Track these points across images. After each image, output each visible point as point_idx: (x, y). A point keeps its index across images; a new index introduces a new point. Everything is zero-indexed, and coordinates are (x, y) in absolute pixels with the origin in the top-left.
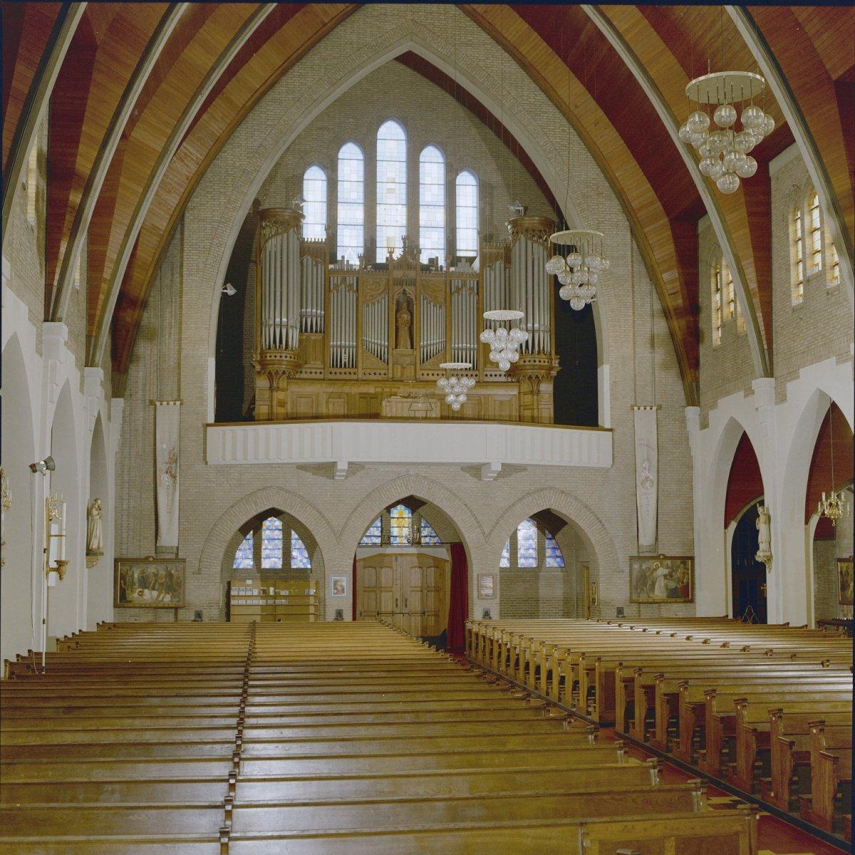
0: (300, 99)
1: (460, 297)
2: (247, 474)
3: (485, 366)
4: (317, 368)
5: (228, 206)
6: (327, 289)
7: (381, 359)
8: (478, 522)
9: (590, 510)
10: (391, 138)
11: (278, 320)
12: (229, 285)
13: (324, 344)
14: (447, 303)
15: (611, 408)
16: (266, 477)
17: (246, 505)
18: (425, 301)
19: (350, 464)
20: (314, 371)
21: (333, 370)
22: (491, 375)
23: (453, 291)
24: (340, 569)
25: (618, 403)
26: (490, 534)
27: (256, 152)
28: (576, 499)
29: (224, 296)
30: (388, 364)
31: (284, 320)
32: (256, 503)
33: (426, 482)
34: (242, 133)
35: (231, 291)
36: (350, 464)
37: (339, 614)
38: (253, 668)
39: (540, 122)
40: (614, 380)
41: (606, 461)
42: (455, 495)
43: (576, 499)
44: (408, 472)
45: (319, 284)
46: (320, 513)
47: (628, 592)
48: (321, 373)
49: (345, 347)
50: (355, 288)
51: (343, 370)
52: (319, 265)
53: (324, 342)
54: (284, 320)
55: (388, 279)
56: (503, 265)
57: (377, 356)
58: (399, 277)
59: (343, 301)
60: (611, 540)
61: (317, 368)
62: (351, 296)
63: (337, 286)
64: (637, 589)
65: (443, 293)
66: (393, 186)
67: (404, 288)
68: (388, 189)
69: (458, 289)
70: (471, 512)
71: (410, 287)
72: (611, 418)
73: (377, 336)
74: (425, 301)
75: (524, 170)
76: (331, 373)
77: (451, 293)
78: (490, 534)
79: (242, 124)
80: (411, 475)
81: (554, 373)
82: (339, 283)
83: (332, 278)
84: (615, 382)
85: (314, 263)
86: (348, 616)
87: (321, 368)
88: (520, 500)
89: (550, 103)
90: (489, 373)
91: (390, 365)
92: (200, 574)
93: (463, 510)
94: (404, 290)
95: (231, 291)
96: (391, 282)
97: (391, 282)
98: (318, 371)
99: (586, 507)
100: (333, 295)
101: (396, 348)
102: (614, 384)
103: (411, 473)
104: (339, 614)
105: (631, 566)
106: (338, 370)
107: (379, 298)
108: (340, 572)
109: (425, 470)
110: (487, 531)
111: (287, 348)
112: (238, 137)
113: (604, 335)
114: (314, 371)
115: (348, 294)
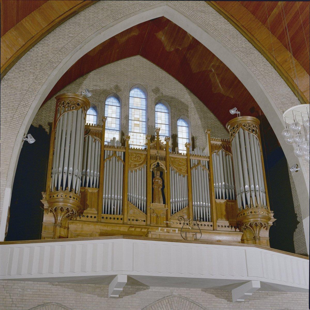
0: (93, 25)
1: (197, 170)
2: (29, 290)
3: (217, 219)
4: (93, 214)
5: (35, 81)
6: (102, 159)
7: (141, 209)
10: (137, 99)
11: (66, 168)
12: (29, 135)
13: (98, 195)
18: (173, 172)
19: (129, 278)
20: (90, 215)
21: (105, 216)
23: (192, 166)
27: (60, 51)
29: (26, 143)
30: (146, 214)
34: (51, 38)
35: (31, 140)
36: (129, 278)
39: (250, 58)
44: (172, 293)
45: (97, 154)
48: (95, 217)
49: (115, 199)
50: (122, 159)
51: (112, 216)
52: (97, 142)
53: (99, 194)
54: (71, 169)
55: (147, 155)
56: (224, 153)
57: (139, 208)
58: (154, 154)
59: (114, 168)
61: (93, 214)
62: (120, 165)
65: (185, 167)
66: (138, 123)
67: (158, 160)
68: (135, 124)
69: (195, 166)
71: (162, 161)
73: (138, 193)
74: (173, 172)
75: (217, 120)
76: (103, 218)
77: (191, 168)
79: (51, 33)
81: (271, 223)
82: (111, 155)
83: (106, 151)
85: (93, 140)
87: (95, 214)
89: (255, 49)
91: (149, 214)
94: (158, 163)
95: (31, 140)
96: (149, 157)
97: (149, 157)
98: (93, 216)
100: (107, 163)
101: (152, 202)
103: (174, 294)
106: (109, 216)
107: (141, 167)
109: (187, 291)
111: (71, 191)
112: (48, 40)
114: (90, 215)
115: (117, 163)
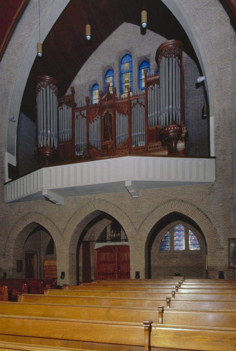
8: (132, 223)
9: (200, 210)
14: (129, 113)
15: (215, 144)
16: (30, 207)
17: (22, 222)
22: (152, 147)
24: (63, 251)
25: (220, 140)
26: (139, 229)
28: (191, 204)
31: (49, 131)
32: (26, 220)
33: (104, 202)
37: (137, 274)
38: (182, 286)
40: (217, 126)
41: (211, 177)
42: (119, 208)
43: (191, 204)
44: (95, 198)
46: (54, 223)
47: (227, 261)
60: (215, 228)
63: (77, 116)
64: (233, 260)
70: (128, 217)
72: (215, 151)
78: (139, 229)
80: (96, 200)
84: (218, 127)
86: (142, 275)
88: (156, 208)
90: (151, 146)
92: (5, 255)
93: (124, 216)
99: (198, 209)
102: (217, 128)
104: (137, 274)
105: (229, 245)
108: (63, 253)
110: (137, 228)
113: (209, 97)
